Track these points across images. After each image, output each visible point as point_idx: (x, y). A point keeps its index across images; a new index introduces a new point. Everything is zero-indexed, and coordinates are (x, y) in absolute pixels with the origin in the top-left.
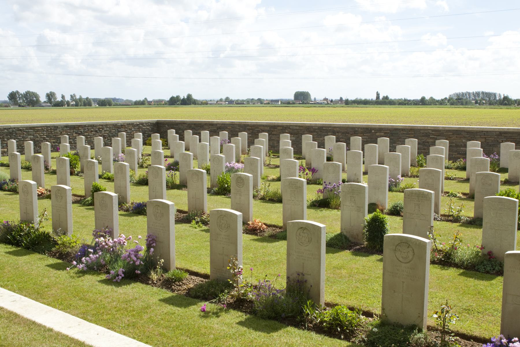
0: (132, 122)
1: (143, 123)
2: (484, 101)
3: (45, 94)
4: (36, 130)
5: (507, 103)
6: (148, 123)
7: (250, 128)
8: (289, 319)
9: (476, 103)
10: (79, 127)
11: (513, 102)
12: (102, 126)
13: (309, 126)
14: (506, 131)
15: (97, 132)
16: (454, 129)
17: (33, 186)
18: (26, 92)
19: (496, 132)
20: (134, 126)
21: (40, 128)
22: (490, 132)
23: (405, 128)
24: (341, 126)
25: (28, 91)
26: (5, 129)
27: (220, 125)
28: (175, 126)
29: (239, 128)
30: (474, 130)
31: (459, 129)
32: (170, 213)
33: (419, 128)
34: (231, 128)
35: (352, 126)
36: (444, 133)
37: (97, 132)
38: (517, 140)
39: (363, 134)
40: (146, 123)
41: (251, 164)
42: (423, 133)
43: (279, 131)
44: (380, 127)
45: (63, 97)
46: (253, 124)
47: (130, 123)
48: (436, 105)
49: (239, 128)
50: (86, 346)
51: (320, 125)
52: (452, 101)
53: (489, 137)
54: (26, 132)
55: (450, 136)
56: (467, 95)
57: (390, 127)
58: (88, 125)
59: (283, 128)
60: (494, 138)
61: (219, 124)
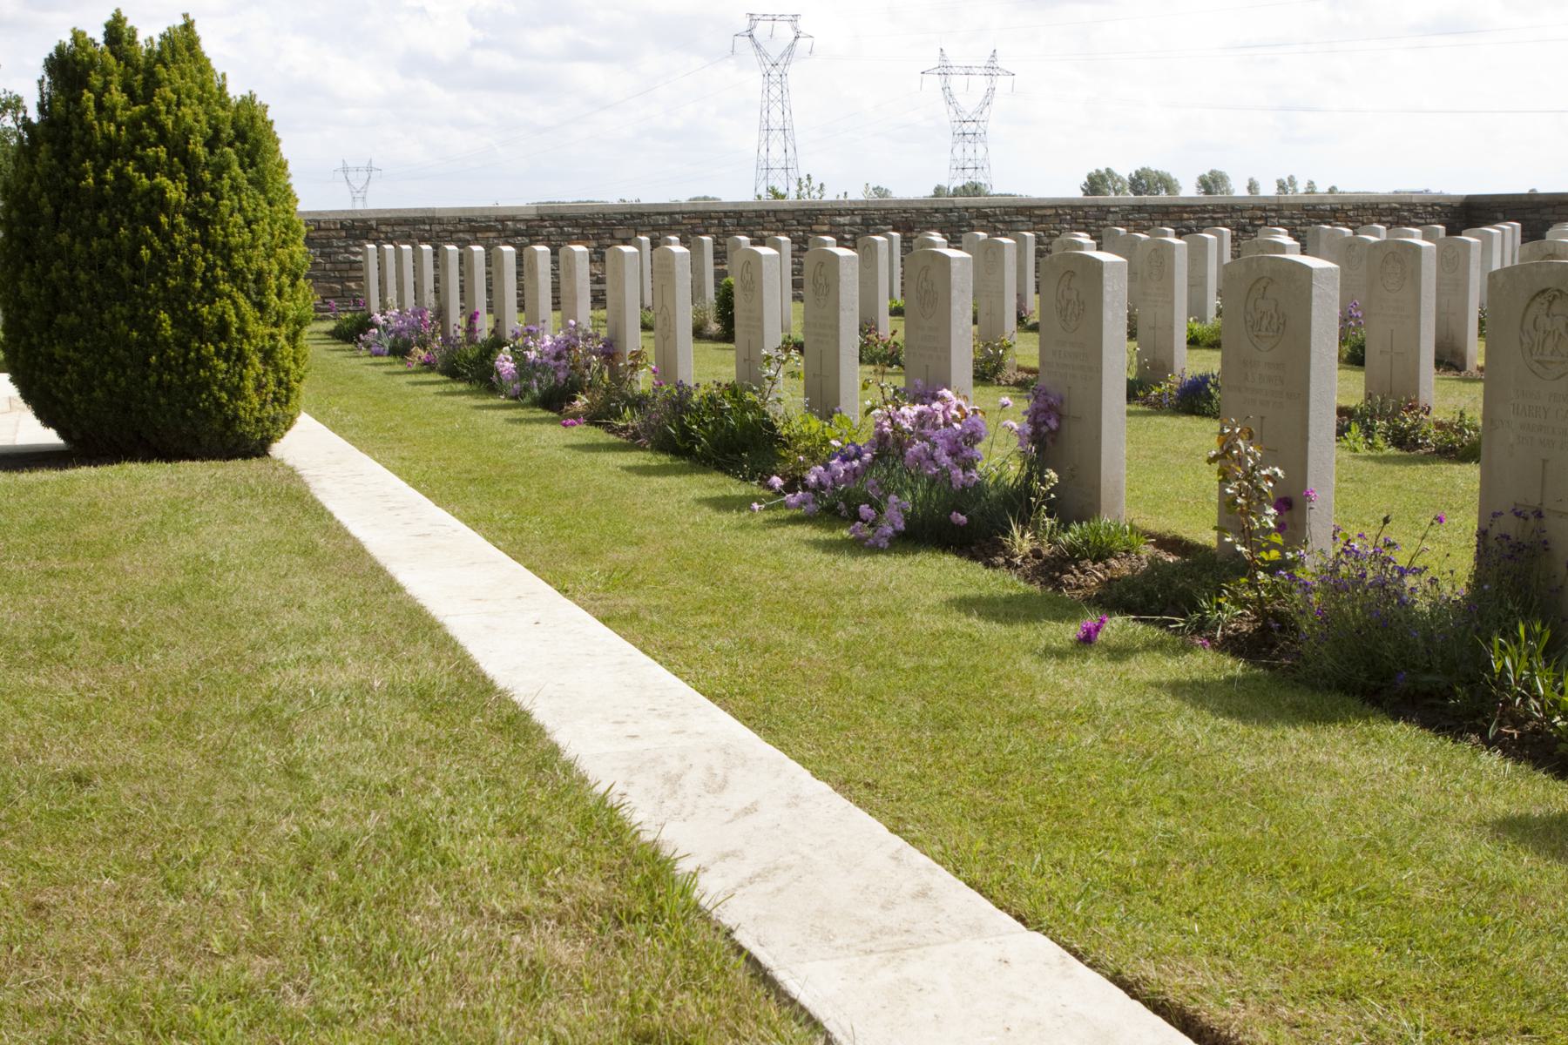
0: (1373, 201)
1: (1415, 204)
3: (1195, 181)
4: (1038, 216)
6: (1433, 205)
8: (1429, 701)
10: (1182, 212)
12: (1264, 209)
15: (1245, 231)
17: (764, 263)
18: (1137, 172)
20: (1381, 215)
21: (1049, 212)
25: (1143, 169)
26: (937, 210)
28: (1530, 216)
32: (1107, 298)
37: (1245, 231)
40: (1425, 206)
45: (1252, 186)
47: (1364, 205)
54: (1004, 222)
58: (1213, 205)
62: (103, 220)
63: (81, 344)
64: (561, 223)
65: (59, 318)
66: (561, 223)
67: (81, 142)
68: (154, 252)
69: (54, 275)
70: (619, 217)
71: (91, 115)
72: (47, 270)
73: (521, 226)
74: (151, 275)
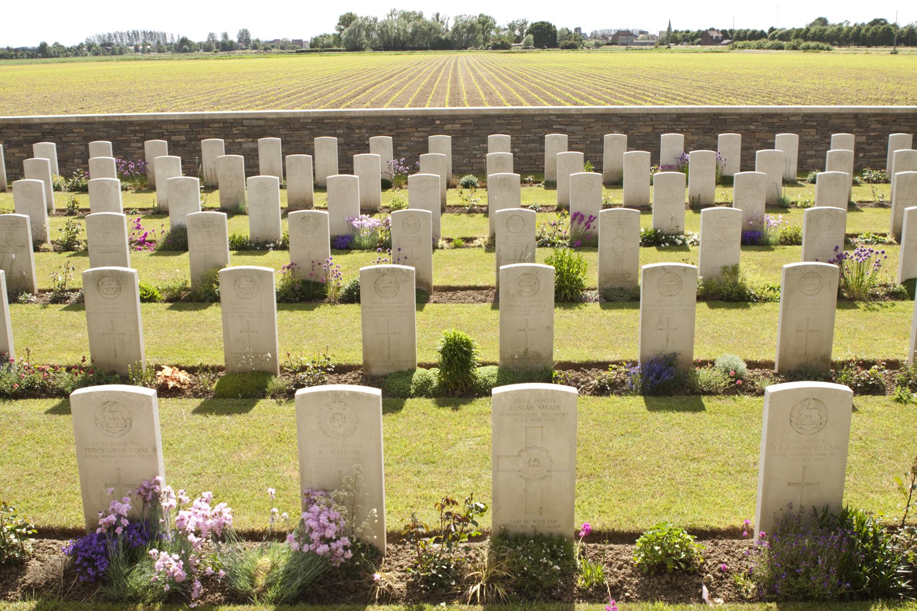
2: (149, 47)
5: (188, 48)
7: (138, 128)
9: (137, 50)
11: (197, 46)
13: (289, 119)
14: (687, 111)
16: (598, 112)
19: (670, 114)
22: (661, 114)
23: (504, 113)
24: (367, 114)
27: (53, 127)
29: (106, 129)
30: (634, 112)
31: (607, 112)
33: (532, 112)
34: (83, 130)
35: (391, 114)
36: (580, 120)
38: (706, 126)
39: (417, 129)
41: (620, 225)
42: (539, 122)
43: (216, 132)
44: (453, 113)
46: (143, 119)
48: (67, 56)
49: (106, 129)
50: (738, 610)
51: (316, 115)
52: (94, 48)
53: (660, 123)
55: (591, 125)
56: (118, 38)
57: (472, 113)
59: (225, 125)
60: (669, 125)
61: (47, 124)
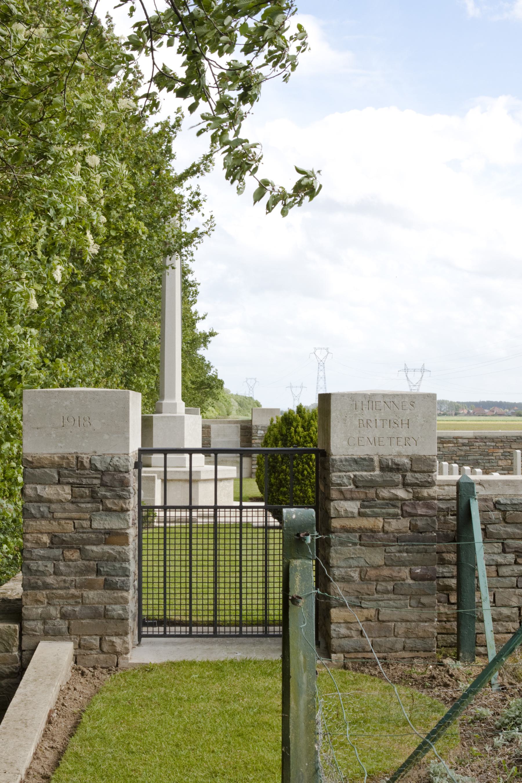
62: (295, 463)
63: (287, 496)
64: (485, 440)
65: (281, 489)
66: (485, 440)
67: (290, 441)
68: (308, 473)
69: (281, 477)
70: (514, 438)
71: (293, 434)
72: (279, 476)
73: (466, 441)
74: (307, 477)
